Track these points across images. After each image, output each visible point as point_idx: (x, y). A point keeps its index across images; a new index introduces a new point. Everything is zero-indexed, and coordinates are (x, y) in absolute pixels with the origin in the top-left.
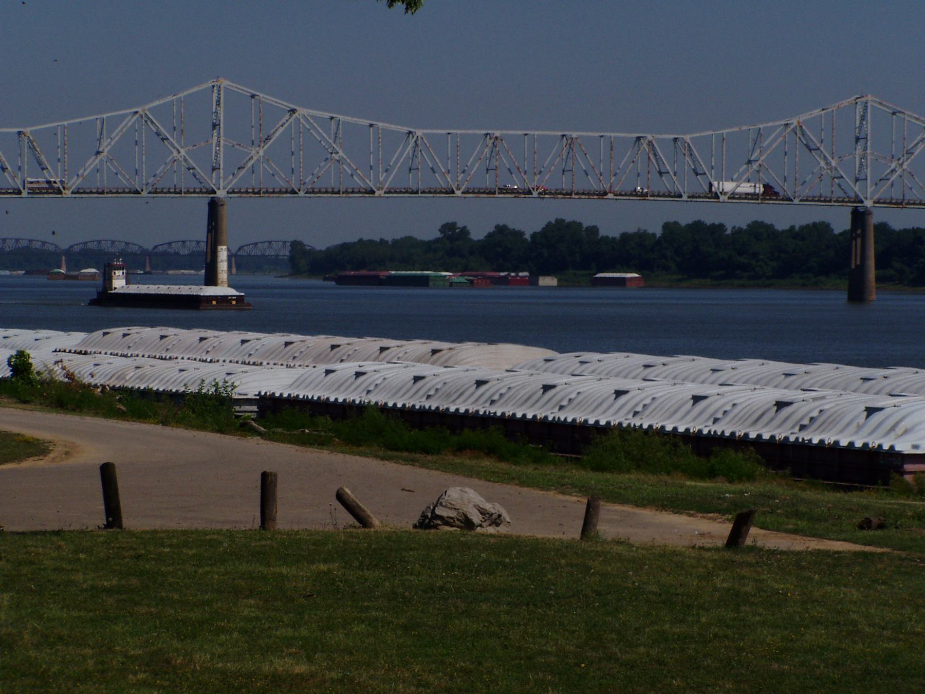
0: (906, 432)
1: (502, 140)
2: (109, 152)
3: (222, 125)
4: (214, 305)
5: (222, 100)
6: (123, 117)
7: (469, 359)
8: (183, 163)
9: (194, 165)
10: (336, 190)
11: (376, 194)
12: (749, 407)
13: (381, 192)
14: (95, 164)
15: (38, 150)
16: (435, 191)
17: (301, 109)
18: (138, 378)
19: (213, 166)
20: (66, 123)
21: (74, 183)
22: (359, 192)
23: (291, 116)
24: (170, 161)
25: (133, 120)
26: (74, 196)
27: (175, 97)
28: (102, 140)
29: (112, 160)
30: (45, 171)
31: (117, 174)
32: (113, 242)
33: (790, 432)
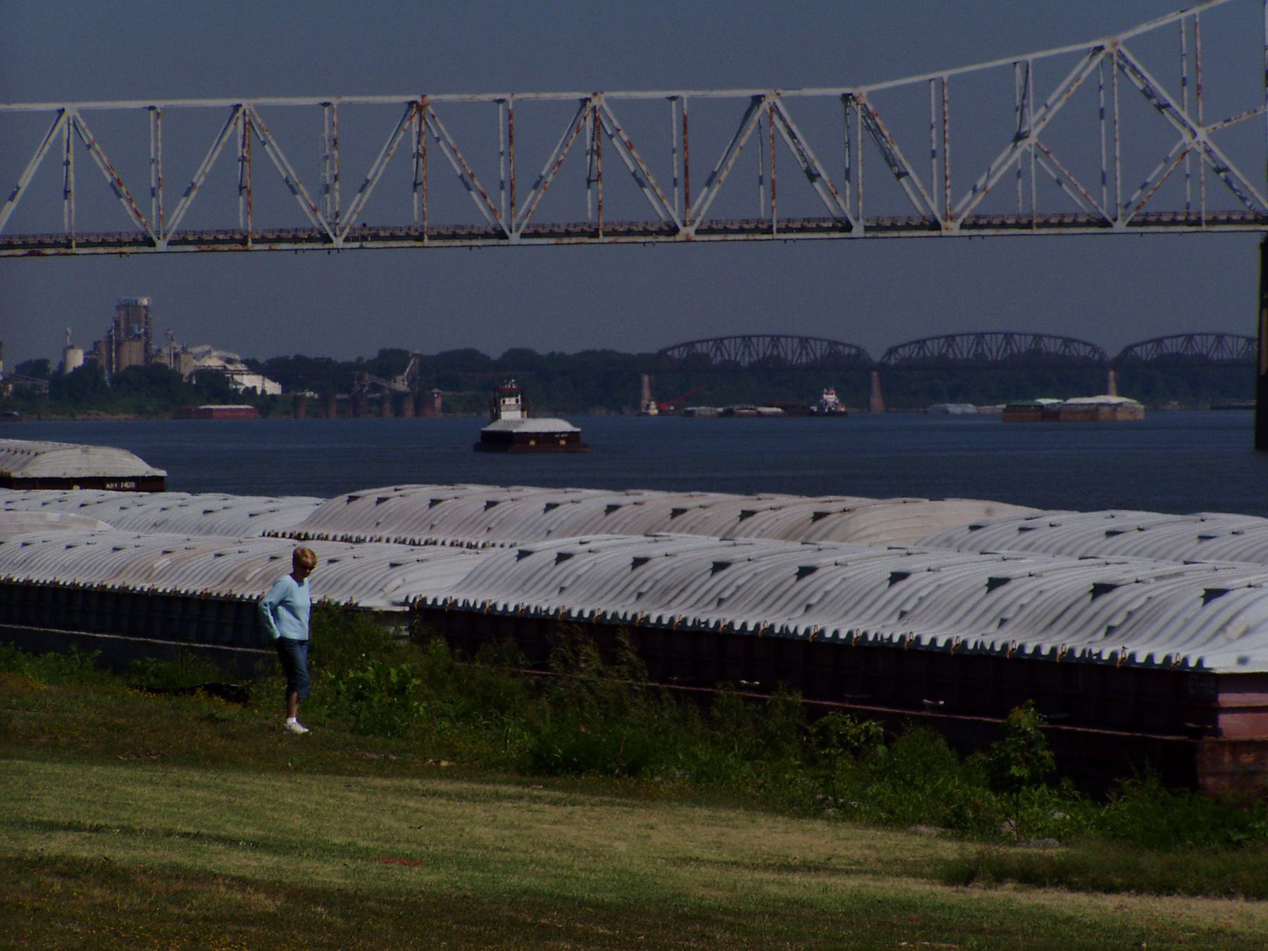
0: (1247, 632)
2: (1040, 136)
4: (562, 446)
6: (1074, 58)
7: (871, 531)
8: (1204, 156)
9: (1227, 163)
10: (1024, 221)
12: (1054, 598)
14: (1010, 162)
15: (886, 133)
18: (263, 577)
20: (945, 74)
21: (968, 205)
26: (966, 232)
27: (1183, 15)
28: (1026, 110)
29: (1047, 153)
30: (903, 180)
31: (1059, 182)
32: (1220, 337)
33: (1087, 641)
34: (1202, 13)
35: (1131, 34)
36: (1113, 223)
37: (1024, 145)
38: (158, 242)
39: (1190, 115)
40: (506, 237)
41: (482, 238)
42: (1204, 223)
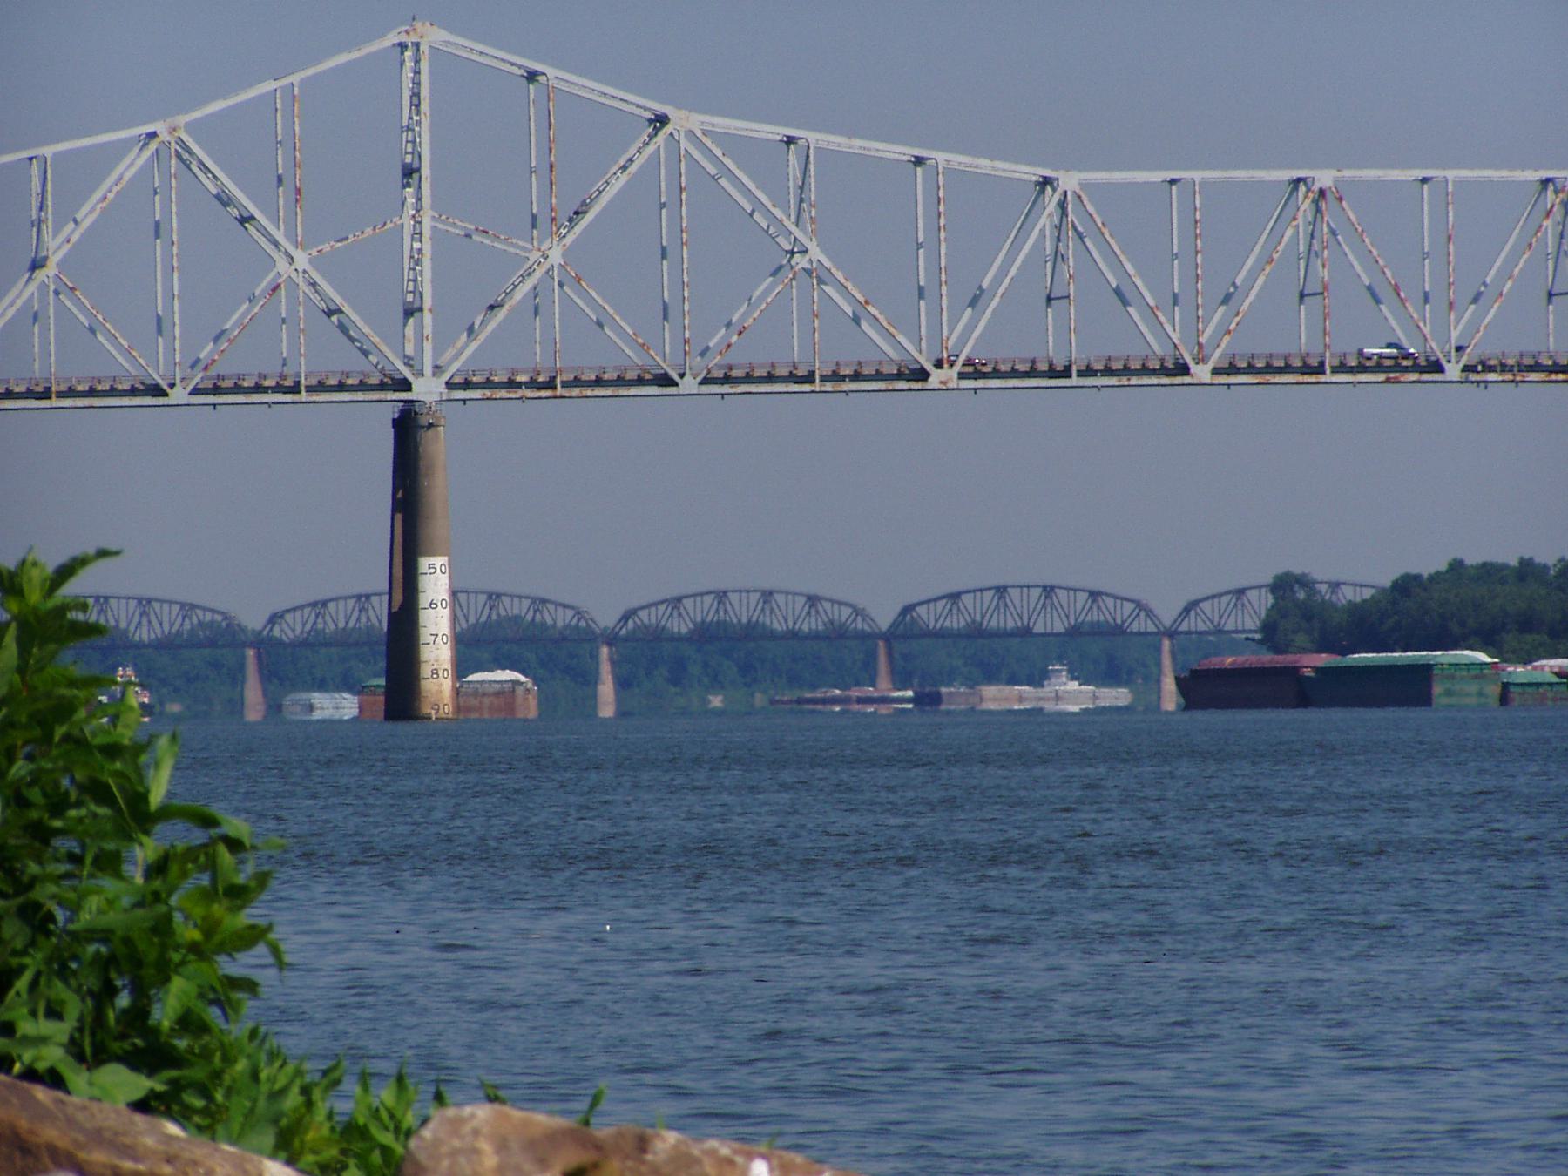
1: (1340, 199)
3: (426, 171)
5: (425, 92)
9: (338, 300)
11: (933, 382)
13: (949, 375)
16: (1126, 368)
17: (683, 113)
19: (405, 302)
22: (878, 376)
23: (657, 130)
24: (263, 291)
25: (140, 161)
28: (44, 227)
29: (72, 289)
34: (302, 81)
35: (197, 114)
36: (169, 391)
37: (40, 275)
38: (1447, 366)
39: (287, 236)
40: (1441, 370)
41: (851, 381)
42: (53, 395)
